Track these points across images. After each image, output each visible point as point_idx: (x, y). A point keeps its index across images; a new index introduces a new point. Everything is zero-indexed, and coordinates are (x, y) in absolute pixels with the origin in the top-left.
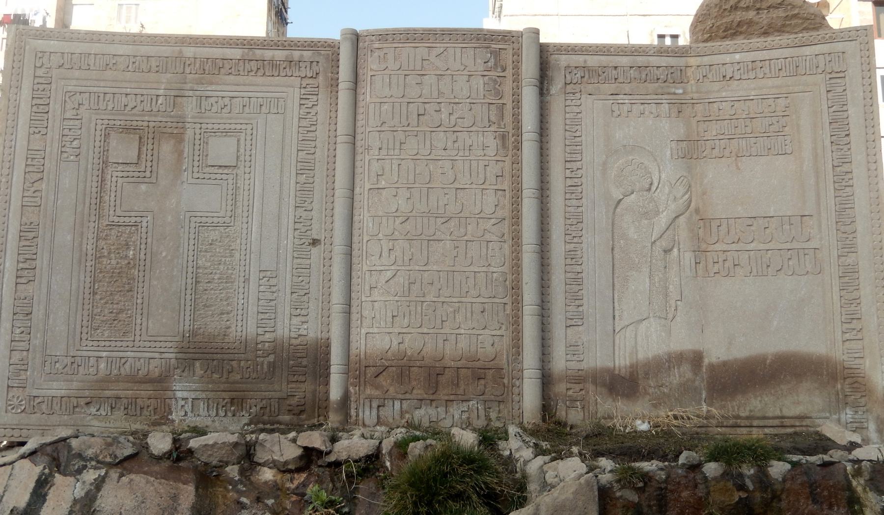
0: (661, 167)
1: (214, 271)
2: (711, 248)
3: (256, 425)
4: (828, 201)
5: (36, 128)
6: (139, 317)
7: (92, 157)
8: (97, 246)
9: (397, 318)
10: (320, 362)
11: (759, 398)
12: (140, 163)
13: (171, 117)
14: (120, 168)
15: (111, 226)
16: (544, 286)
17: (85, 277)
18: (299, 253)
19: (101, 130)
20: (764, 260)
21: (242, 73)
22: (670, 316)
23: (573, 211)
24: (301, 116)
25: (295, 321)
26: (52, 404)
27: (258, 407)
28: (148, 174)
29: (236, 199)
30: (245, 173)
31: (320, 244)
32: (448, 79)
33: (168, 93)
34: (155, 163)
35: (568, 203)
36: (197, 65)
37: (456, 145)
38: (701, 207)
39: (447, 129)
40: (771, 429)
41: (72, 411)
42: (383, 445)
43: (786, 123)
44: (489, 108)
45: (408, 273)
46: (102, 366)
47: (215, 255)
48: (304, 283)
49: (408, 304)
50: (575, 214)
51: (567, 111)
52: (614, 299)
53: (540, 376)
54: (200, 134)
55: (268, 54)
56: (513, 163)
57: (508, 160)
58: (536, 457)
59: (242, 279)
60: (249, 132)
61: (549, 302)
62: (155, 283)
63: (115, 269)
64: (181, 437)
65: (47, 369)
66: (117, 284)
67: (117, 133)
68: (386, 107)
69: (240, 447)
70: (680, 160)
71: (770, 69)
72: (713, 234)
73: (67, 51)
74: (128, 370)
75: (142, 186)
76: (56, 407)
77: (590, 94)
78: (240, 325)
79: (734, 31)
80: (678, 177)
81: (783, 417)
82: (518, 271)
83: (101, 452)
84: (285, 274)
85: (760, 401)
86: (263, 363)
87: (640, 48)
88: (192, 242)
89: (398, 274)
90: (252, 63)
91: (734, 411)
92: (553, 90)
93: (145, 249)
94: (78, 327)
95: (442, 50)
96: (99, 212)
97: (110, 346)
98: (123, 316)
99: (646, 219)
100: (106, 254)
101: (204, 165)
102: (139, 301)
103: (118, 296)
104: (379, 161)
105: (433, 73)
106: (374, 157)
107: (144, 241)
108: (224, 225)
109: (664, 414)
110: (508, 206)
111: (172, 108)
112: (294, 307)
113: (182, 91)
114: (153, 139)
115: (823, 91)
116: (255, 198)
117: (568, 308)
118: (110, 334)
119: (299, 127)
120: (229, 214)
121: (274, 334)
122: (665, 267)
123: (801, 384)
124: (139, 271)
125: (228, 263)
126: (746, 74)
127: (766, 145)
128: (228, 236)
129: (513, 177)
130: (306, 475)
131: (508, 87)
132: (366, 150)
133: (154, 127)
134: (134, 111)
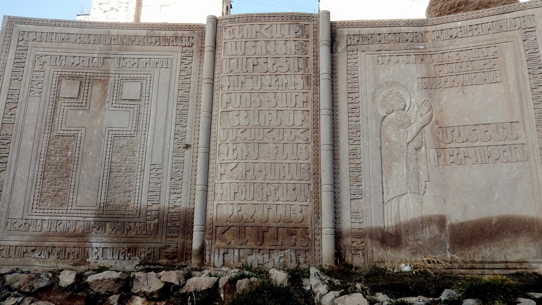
0: (411, 95)
1: (122, 165)
2: (448, 146)
3: (144, 265)
4: (530, 112)
5: (16, 76)
6: (71, 194)
7: (49, 94)
8: (48, 149)
9: (238, 194)
10: (188, 224)
11: (488, 248)
12: (79, 97)
13: (101, 70)
14: (67, 101)
15: (58, 136)
16: (335, 173)
17: (39, 168)
18: (177, 153)
19: (56, 78)
20: (486, 153)
21: (146, 44)
22: (422, 192)
23: (354, 124)
24: (181, 69)
25: (173, 197)
26: (9, 251)
27: (146, 254)
28: (84, 104)
29: (138, 120)
30: (145, 104)
31: (191, 148)
32: (272, 43)
33: (100, 56)
34: (88, 98)
35: (350, 119)
36: (119, 40)
37: (277, 83)
38: (439, 119)
39: (272, 74)
40: (499, 271)
41: (22, 255)
42: (220, 281)
43: (496, 63)
44: (298, 60)
45: (245, 164)
46: (45, 226)
47: (123, 154)
48: (179, 172)
49: (245, 185)
50: (355, 126)
51: (349, 62)
52: (382, 181)
53: (333, 233)
54: (118, 80)
55: (163, 33)
56: (314, 94)
57: (311, 92)
58: (329, 291)
59: (140, 170)
60: (149, 79)
61: (339, 183)
62: (84, 172)
63: (59, 163)
64: (85, 274)
65: (8, 228)
66: (59, 173)
67: (66, 79)
68: (233, 61)
69: (121, 282)
70: (424, 90)
71: (482, 29)
72: (448, 137)
73: (39, 31)
74: (62, 228)
75: (80, 112)
76: (12, 253)
77: (363, 51)
78: (136, 199)
79: (456, 9)
80: (423, 101)
81: (507, 262)
82: (318, 163)
83: (24, 284)
84: (167, 166)
85: (490, 250)
86: (150, 224)
87: (395, 22)
88: (109, 146)
89: (239, 165)
90: (153, 38)
91: (470, 257)
92: (339, 50)
93: (79, 151)
94: (32, 200)
95: (269, 26)
96: (51, 128)
97: (51, 213)
98: (61, 193)
99: (403, 128)
100: (53, 154)
101: (119, 99)
102: (73, 184)
103: (59, 180)
104: (228, 94)
105: (262, 40)
106: (225, 92)
107: (78, 145)
108: (130, 136)
109: (420, 260)
110: (311, 121)
111: (102, 65)
112: (172, 187)
113: (109, 55)
114: (89, 83)
115: (520, 40)
116: (151, 119)
117: (352, 187)
118: (52, 205)
119: (180, 76)
120: (134, 129)
121: (159, 205)
122: (417, 160)
123: (519, 238)
124: (74, 165)
125: (131, 160)
126: (466, 34)
127: (482, 77)
128: (132, 143)
129: (314, 102)
130: (165, 302)
131: (310, 48)
132: (220, 88)
133: (90, 76)
134: (78, 67)
